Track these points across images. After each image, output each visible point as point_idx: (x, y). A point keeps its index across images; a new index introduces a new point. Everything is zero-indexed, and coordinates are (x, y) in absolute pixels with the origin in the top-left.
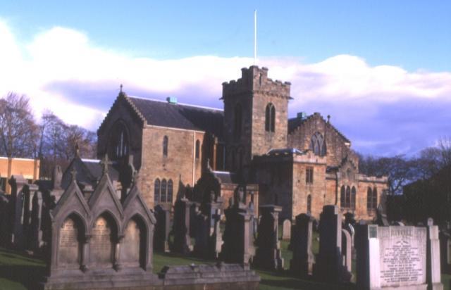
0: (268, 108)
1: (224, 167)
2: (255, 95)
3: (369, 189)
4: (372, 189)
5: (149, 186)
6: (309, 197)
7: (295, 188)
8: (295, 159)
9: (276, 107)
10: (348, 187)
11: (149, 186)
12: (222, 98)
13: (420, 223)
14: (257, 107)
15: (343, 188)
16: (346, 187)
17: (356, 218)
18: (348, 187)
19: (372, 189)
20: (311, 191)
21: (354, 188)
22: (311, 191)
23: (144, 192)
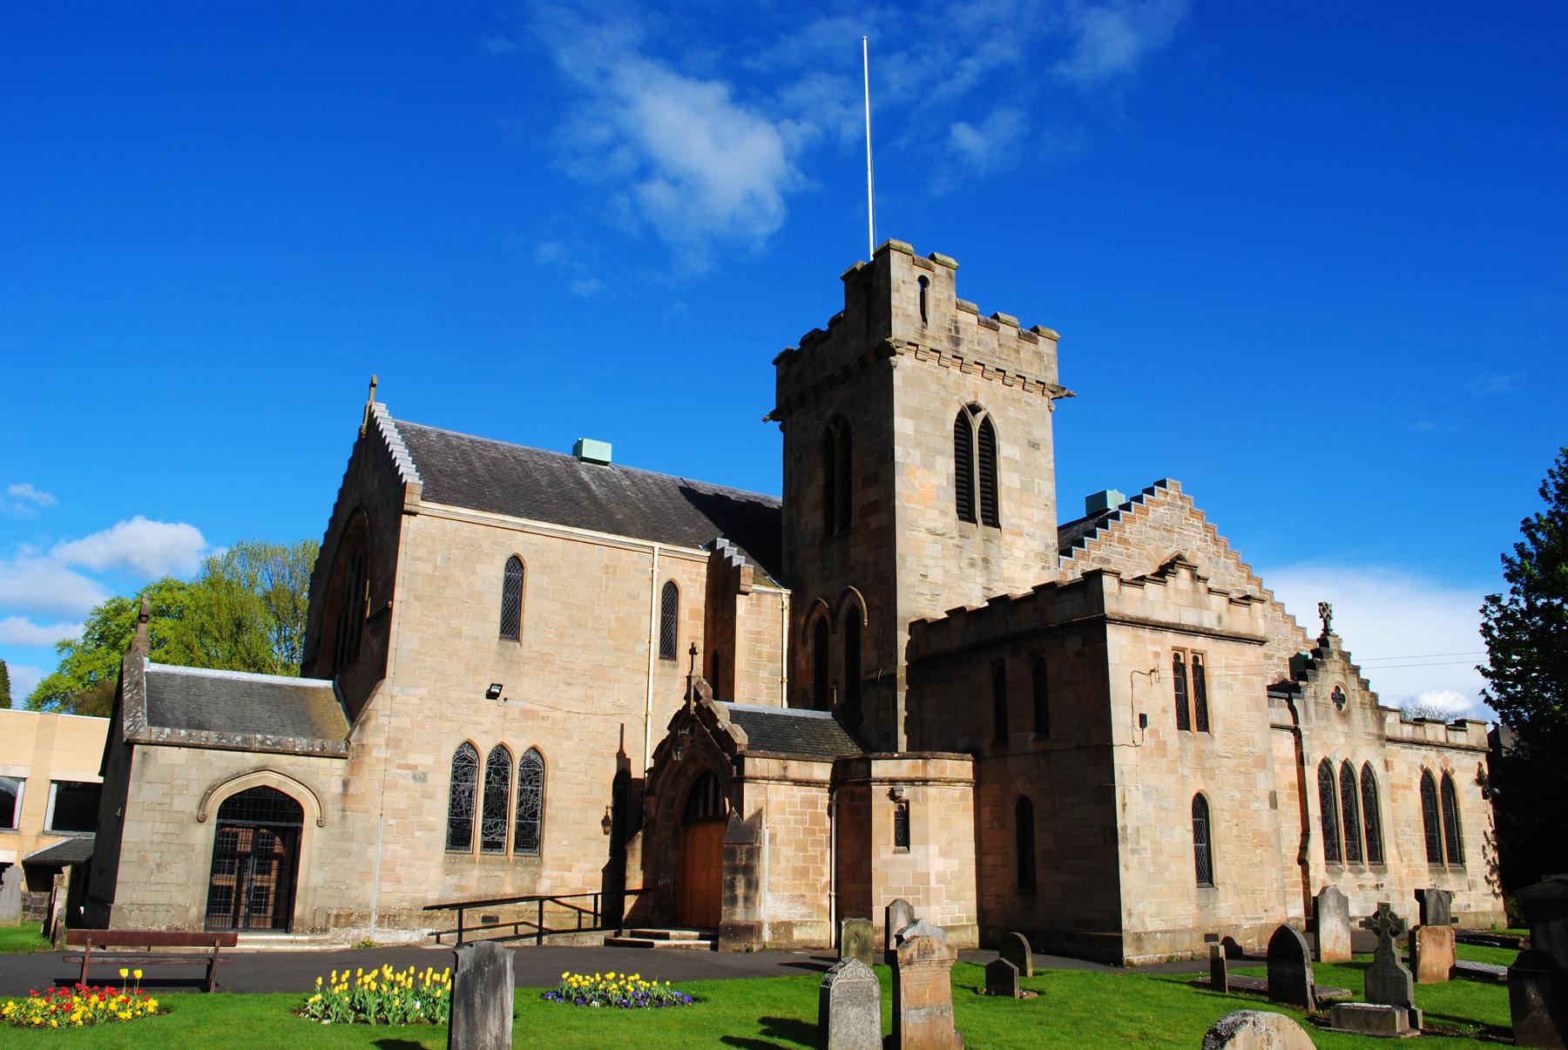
0: (962, 423)
1: (902, 739)
2: (903, 364)
3: (1427, 776)
4: (1438, 776)
5: (422, 778)
6: (1200, 806)
7: (1124, 758)
8: (1110, 607)
9: (997, 422)
10: (1347, 767)
11: (422, 778)
12: (774, 416)
13: (986, 811)
14: (915, 414)
15: (1325, 768)
16: (1337, 768)
17: (1456, 906)
18: (1347, 767)
19: (1438, 776)
20: (1209, 774)
21: (1367, 768)
22: (1209, 774)
23: (397, 800)
